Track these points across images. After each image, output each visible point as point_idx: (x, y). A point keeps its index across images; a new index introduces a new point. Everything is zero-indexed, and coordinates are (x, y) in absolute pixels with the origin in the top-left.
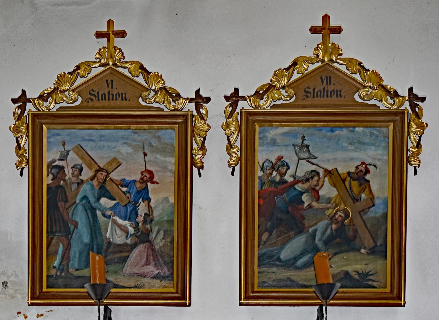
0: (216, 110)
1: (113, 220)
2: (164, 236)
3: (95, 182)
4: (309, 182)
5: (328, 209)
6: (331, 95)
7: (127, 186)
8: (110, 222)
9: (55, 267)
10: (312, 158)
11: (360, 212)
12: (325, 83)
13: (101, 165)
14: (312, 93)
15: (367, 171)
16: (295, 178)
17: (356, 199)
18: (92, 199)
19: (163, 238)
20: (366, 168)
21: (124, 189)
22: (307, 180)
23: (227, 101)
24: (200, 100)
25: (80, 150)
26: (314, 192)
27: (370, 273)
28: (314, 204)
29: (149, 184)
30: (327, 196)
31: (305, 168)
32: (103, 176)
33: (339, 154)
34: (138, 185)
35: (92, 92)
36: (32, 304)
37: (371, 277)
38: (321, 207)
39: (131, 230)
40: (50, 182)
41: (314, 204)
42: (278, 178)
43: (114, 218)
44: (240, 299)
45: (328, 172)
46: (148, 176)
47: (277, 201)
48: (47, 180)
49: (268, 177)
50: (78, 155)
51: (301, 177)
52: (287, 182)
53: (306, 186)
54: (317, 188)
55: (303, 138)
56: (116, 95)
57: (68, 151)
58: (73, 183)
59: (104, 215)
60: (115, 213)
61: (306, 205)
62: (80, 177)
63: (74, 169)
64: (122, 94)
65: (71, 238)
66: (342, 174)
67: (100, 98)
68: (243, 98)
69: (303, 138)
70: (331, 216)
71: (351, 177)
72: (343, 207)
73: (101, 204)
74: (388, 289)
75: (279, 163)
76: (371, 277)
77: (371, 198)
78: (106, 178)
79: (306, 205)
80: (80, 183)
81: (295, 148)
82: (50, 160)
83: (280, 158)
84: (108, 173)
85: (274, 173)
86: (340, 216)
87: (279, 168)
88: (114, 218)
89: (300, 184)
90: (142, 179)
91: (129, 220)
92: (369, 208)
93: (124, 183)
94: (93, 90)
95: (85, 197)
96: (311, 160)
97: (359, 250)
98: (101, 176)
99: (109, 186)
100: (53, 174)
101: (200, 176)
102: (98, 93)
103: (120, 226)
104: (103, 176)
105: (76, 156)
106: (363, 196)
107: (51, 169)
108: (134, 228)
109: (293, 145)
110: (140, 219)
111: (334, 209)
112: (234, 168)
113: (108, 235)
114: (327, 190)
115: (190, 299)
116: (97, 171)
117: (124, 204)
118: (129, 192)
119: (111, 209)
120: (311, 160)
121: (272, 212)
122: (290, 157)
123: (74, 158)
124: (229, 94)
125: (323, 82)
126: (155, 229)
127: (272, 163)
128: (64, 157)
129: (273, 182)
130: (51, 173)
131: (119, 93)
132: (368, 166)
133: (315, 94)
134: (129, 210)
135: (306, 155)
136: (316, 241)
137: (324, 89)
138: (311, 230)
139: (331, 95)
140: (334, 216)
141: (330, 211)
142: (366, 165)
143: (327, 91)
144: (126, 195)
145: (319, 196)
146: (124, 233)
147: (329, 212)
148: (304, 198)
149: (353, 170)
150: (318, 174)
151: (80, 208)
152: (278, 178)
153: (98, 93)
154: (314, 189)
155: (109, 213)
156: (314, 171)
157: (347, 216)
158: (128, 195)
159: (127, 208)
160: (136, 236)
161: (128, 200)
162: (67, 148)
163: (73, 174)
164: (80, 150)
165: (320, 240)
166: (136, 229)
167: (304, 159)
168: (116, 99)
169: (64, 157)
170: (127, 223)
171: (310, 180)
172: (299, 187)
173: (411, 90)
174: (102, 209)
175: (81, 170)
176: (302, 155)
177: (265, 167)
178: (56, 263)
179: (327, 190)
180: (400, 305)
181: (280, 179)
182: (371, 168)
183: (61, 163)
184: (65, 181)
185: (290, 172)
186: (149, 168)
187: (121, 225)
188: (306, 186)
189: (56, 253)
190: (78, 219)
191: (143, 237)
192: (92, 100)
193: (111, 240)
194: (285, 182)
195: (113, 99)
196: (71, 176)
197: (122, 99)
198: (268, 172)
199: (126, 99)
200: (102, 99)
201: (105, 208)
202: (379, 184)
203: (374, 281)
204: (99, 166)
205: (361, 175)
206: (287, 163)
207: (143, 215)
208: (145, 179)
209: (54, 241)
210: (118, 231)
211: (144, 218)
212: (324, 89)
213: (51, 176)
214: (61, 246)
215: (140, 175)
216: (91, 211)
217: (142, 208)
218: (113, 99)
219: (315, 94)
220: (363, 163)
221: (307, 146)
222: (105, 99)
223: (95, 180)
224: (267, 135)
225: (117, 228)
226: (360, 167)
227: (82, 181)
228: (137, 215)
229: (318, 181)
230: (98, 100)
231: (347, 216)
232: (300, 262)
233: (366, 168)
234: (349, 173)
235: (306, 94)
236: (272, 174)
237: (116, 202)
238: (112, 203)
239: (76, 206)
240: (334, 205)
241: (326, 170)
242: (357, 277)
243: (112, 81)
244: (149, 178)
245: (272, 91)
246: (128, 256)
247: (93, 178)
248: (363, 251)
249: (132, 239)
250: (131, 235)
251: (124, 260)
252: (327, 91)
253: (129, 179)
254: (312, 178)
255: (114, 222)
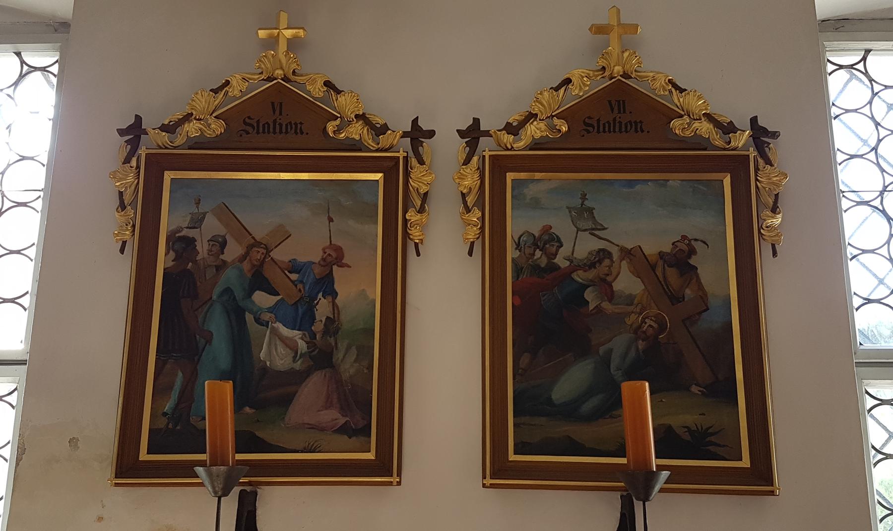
0: (447, 146)
1: (273, 328)
2: (358, 355)
3: (246, 266)
4: (595, 268)
5: (629, 314)
6: (626, 127)
7: (298, 273)
8: (268, 332)
9: (165, 414)
10: (599, 230)
11: (683, 321)
12: (616, 110)
13: (258, 238)
14: (596, 125)
15: (692, 252)
16: (571, 261)
17: (676, 299)
18: (239, 294)
19: (355, 361)
20: (689, 245)
21: (294, 277)
22: (592, 265)
23: (462, 137)
24: (418, 135)
25: (225, 213)
26: (605, 286)
27: (710, 431)
28: (606, 305)
29: (335, 268)
30: (627, 292)
31: (587, 246)
32: (260, 254)
33: (642, 222)
34: (317, 270)
35: (247, 120)
36: (117, 485)
37: (713, 439)
38: (616, 311)
39: (302, 346)
40: (171, 264)
41: (606, 305)
42: (544, 262)
43: (275, 325)
44: (484, 477)
45: (627, 253)
46: (334, 255)
47: (542, 299)
48: (163, 260)
49: (528, 259)
50: (220, 220)
51: (583, 260)
52: (560, 267)
53: (591, 274)
54: (609, 279)
55: (584, 197)
56: (287, 125)
57: (205, 214)
58: (209, 266)
59: (258, 320)
60: (276, 317)
61: (591, 306)
62: (222, 257)
63: (211, 243)
64: (296, 124)
65: (199, 360)
66: (650, 255)
67: (601, 129)
68: (487, 134)
69: (584, 197)
70: (634, 326)
71: (665, 261)
72: (655, 311)
73: (253, 302)
74: (746, 463)
75: (546, 237)
76: (713, 439)
77: (701, 297)
78: (264, 258)
79: (591, 306)
80: (221, 267)
81: (570, 212)
82: (173, 227)
83: (547, 229)
84: (268, 251)
85: (538, 253)
86: (650, 326)
87: (545, 244)
88: (275, 325)
89: (580, 272)
90: (324, 260)
91: (299, 330)
92: (700, 313)
93: (295, 267)
94: (249, 118)
95: (228, 291)
96: (596, 232)
97: (688, 389)
98: (257, 254)
99: (272, 274)
100: (176, 251)
101: (418, 254)
102: (598, 121)
103: (284, 340)
104: (260, 254)
105: (216, 222)
106: (688, 292)
107: (173, 244)
108: (307, 343)
109: (568, 208)
110: (318, 327)
111: (640, 314)
112: (472, 244)
113: (262, 355)
114: (627, 282)
115: (399, 474)
116: (250, 248)
117: (293, 302)
118: (302, 282)
119: (270, 310)
120: (596, 232)
121: (544, 320)
122: (563, 227)
123: (212, 226)
124: (464, 127)
125: (612, 110)
126: (342, 346)
127: (534, 237)
128: (197, 222)
129: (536, 269)
130: (173, 250)
131: (290, 123)
132: (693, 242)
133: (261, 129)
134: (300, 311)
135: (590, 225)
136: (612, 371)
137: (614, 119)
138: (602, 350)
139: (626, 127)
140: (640, 327)
141: (633, 317)
142: (690, 241)
143: (281, 125)
144: (296, 286)
145: (612, 291)
146: (289, 351)
147: (631, 320)
148: (589, 295)
149: (667, 248)
150: (609, 255)
151: (218, 309)
152: (544, 262)
153: (598, 121)
154: (604, 280)
155: (266, 316)
156: (603, 250)
157: (662, 327)
158: (300, 286)
159: (297, 308)
160: (310, 357)
161: (300, 295)
162: (204, 207)
163: (210, 250)
164: (225, 213)
165: (618, 369)
166: (311, 344)
167: (585, 230)
168: (287, 132)
169: (197, 222)
170: (295, 334)
171: (597, 265)
172: (579, 277)
173: (754, 120)
174: (255, 309)
175: (223, 244)
176: (582, 224)
177: (522, 244)
178: (168, 407)
179: (627, 282)
180: (772, 493)
181: (547, 265)
182: (698, 246)
183: (191, 233)
184: (195, 262)
185: (564, 251)
186: (336, 241)
187: (287, 338)
188: (591, 274)
189: (171, 388)
190: (213, 328)
191: (321, 358)
192: (248, 133)
193: (268, 363)
194: (557, 268)
195: (281, 132)
196: (206, 255)
197: (296, 133)
198: (528, 251)
199: (302, 133)
200: (264, 132)
201: (260, 309)
202: (358, 288)
203: (719, 446)
204: (253, 238)
205: (681, 259)
206: (557, 237)
207: (324, 320)
208: (329, 259)
209: (168, 366)
210: (281, 349)
211: (325, 325)
212: (614, 119)
213: (172, 254)
214: (180, 374)
215: (321, 253)
216: (236, 313)
217: (323, 308)
218: (281, 132)
219: (623, 126)
220: (684, 237)
221: (590, 211)
222: (269, 132)
223: (245, 262)
224: (526, 191)
225: (278, 342)
226: (678, 244)
227: (224, 262)
228: (313, 319)
229: (610, 267)
230: (258, 133)
231: (662, 327)
232: (587, 407)
233: (689, 245)
234: (661, 255)
235: (585, 128)
236: (534, 255)
237: (279, 298)
238: (274, 299)
239: (212, 305)
240: (640, 306)
241: (623, 250)
242: (687, 437)
243: (281, 104)
244: (336, 259)
245: (532, 123)
246: (296, 392)
247: (242, 258)
248: (695, 389)
249: (302, 363)
250: (302, 355)
251: (286, 401)
252: (620, 123)
253: (302, 259)
254: (600, 262)
255: (275, 332)
